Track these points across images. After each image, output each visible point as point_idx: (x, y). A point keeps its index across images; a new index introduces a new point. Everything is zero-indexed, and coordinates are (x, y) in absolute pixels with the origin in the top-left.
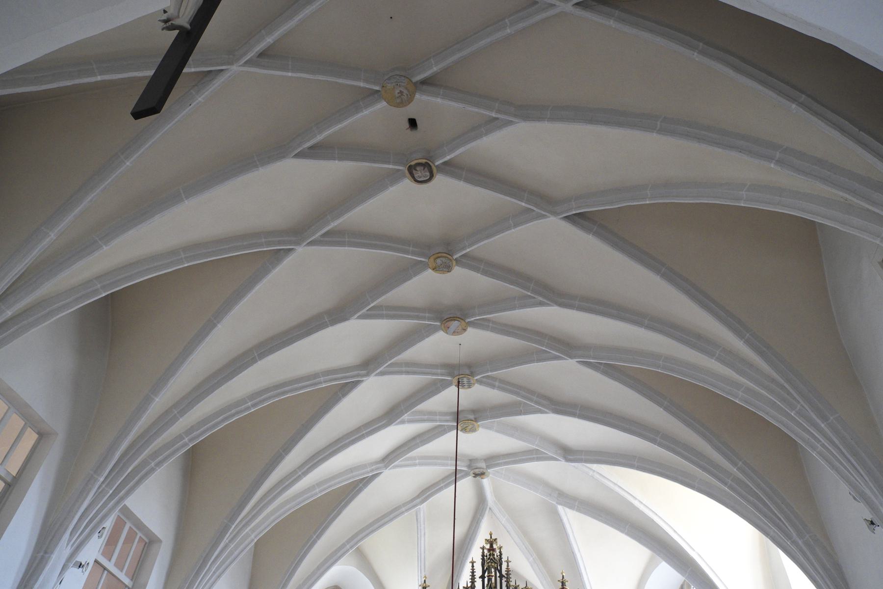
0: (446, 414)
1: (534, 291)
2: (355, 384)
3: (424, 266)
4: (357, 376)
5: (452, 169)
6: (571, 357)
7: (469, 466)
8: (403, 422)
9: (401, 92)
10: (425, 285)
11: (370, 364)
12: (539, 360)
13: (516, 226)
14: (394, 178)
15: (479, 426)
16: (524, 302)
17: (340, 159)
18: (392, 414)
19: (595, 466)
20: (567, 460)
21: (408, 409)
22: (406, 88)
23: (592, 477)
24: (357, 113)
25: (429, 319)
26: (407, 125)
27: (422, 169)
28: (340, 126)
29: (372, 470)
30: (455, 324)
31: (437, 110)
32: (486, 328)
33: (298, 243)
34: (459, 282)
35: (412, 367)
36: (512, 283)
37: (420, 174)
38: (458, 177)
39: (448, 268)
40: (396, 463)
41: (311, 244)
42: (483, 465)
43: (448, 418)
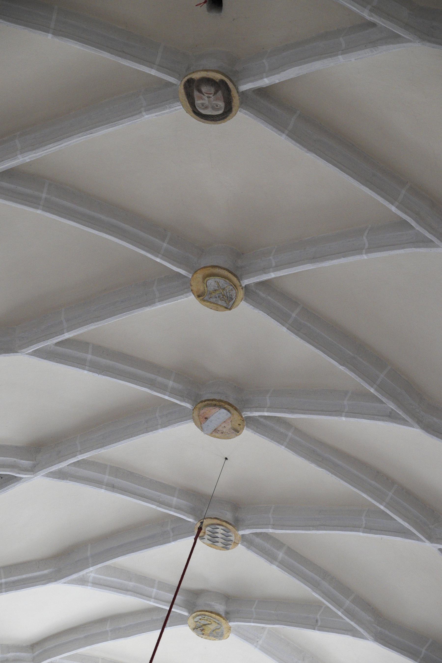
1: (381, 388)
6: (431, 538)
8: (83, 582)
10: (175, 323)
14: (154, 96)
25: (174, 392)
27: (212, 93)
30: (220, 415)
32: (279, 438)
35: (122, 478)
37: (206, 101)
38: (279, 125)
39: (228, 303)
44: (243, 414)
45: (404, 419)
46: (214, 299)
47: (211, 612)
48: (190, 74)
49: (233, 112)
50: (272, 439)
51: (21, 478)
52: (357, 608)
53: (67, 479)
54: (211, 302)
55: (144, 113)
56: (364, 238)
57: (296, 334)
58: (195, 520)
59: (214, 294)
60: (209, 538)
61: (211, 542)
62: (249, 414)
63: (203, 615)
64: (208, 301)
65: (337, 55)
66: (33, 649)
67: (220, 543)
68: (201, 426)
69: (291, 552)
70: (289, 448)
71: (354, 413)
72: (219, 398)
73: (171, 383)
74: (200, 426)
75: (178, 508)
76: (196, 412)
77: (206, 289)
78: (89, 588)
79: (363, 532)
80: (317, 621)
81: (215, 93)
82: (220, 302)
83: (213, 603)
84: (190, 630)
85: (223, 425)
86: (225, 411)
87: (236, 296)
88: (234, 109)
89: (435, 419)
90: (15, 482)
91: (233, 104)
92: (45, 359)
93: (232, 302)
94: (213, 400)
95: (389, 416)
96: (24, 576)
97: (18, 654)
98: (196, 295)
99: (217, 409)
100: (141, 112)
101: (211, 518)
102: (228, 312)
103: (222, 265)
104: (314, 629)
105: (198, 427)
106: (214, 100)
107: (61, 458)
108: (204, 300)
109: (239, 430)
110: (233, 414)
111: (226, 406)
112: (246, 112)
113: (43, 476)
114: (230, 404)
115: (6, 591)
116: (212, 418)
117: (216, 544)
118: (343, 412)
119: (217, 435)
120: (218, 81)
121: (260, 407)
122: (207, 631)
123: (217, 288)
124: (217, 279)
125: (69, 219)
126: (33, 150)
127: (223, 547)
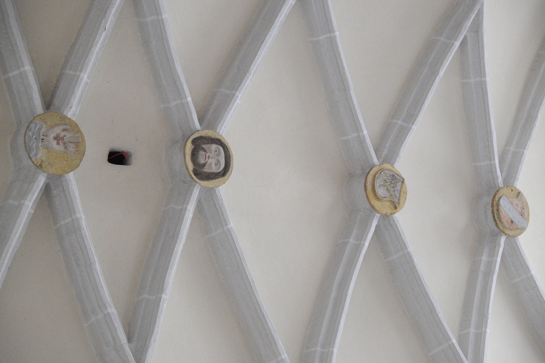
1: (453, 37)
5: (213, 106)
9: (57, 138)
13: (329, 28)
14: (211, 215)
16: (471, 63)
22: (52, 127)
24: (80, 229)
25: (492, 254)
26: (119, 146)
27: (204, 158)
28: (98, 266)
30: (506, 207)
32: (517, 158)
36: (434, 73)
37: (212, 161)
39: (396, 180)
44: (501, 187)
46: (396, 193)
48: (189, 172)
54: (400, 196)
55: (229, 226)
57: (417, 116)
59: (392, 192)
62: (500, 180)
64: (399, 199)
65: (162, 20)
68: (521, 229)
70: (525, 147)
71: (481, 71)
74: (523, 229)
77: (387, 199)
81: (205, 151)
82: (398, 187)
85: (516, 207)
86: (501, 202)
87: (390, 171)
93: (396, 176)
94: (493, 213)
95: (478, 32)
99: (501, 208)
100: (228, 230)
102: (406, 181)
103: (364, 180)
108: (399, 203)
109: (517, 192)
110: (503, 195)
111: (497, 199)
112: (219, 127)
116: (511, 217)
119: (526, 214)
120: (193, 147)
121: (492, 170)
123: (385, 188)
124: (377, 185)
125: (339, 323)
126: (275, 342)
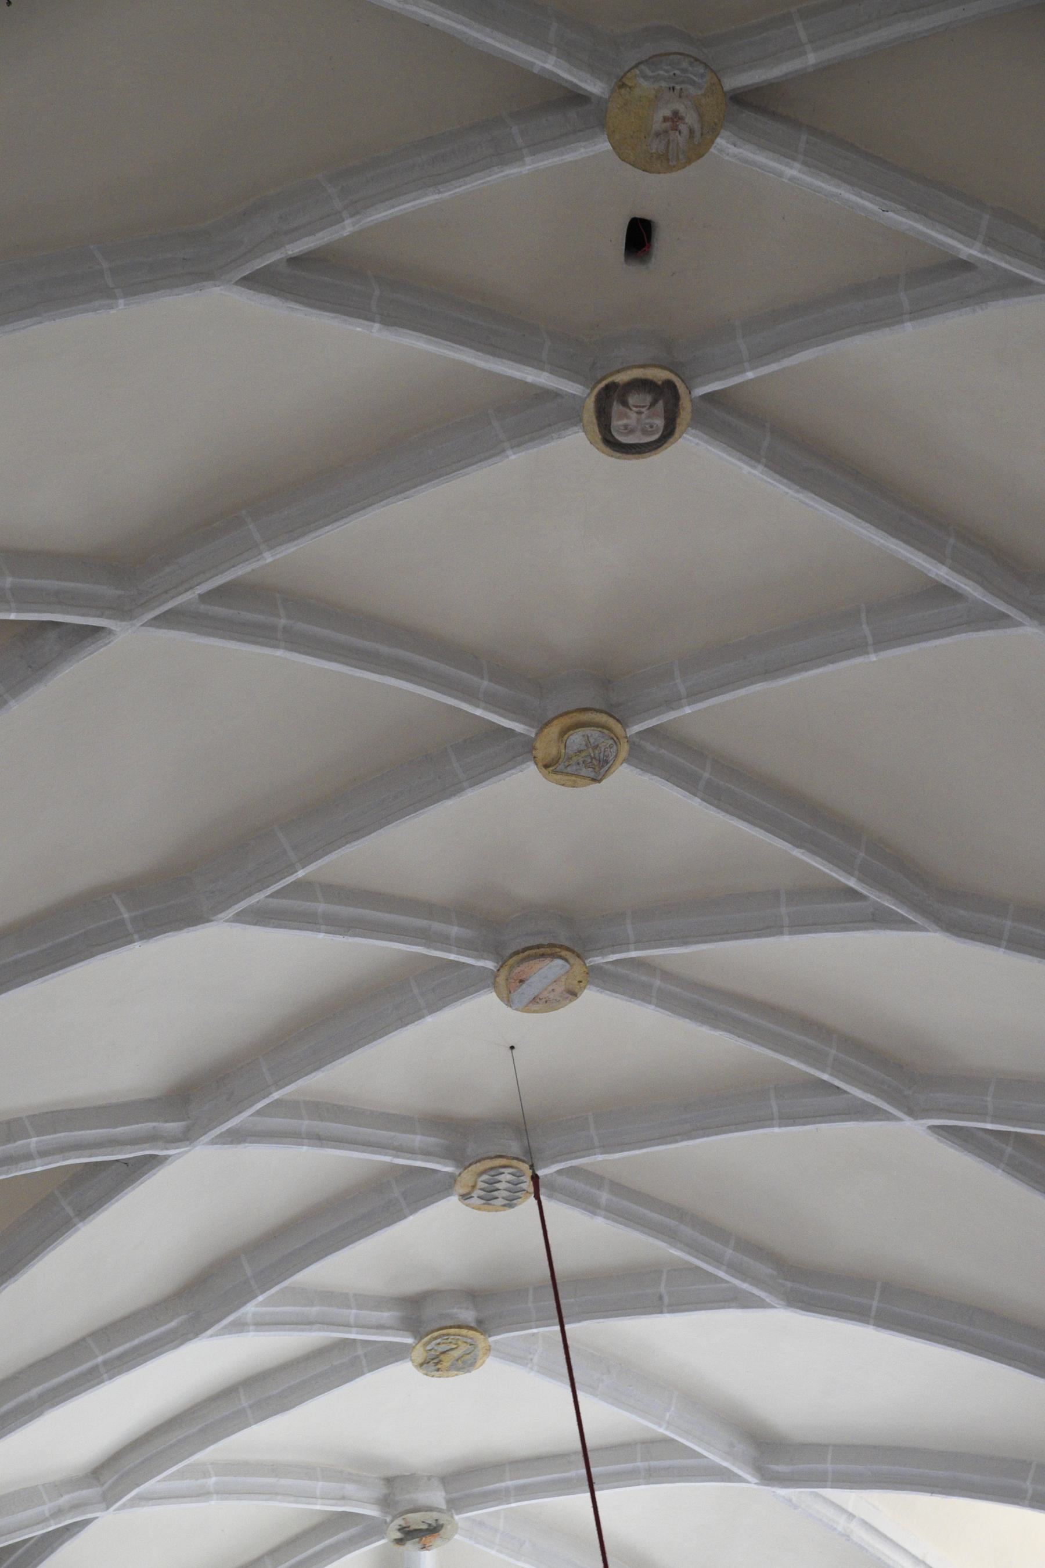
0: (379, 1302)
2: (135, 1170)
3: (515, 750)
4: (152, 1138)
5: (736, 422)
6: (913, 1112)
7: (386, 1503)
8: (239, 1327)
9: (676, 118)
10: (518, 822)
11: (200, 1098)
12: (789, 1119)
13: (882, 643)
14: (529, 417)
15: (488, 1350)
17: (389, 320)
18: (202, 1296)
19: (852, 1499)
20: (768, 1478)
21: (266, 1279)
23: (847, 1537)
27: (638, 405)
28: (431, 198)
29: (58, 1513)
30: (549, 972)
31: (764, 198)
32: (639, 992)
33: (124, 611)
34: (643, 817)
35: (332, 1121)
36: (798, 839)
38: (749, 450)
39: (598, 767)
40: (151, 1485)
41: (170, 619)
42: (437, 1497)
43: (386, 1316)
44: (587, 961)
45: (911, 922)
47: (459, 1327)
48: (612, 374)
49: (676, 435)
50: (633, 997)
51: (166, 1158)
52: (746, 1259)
53: (245, 1141)
54: (567, 774)
56: (864, 626)
58: (457, 1167)
60: (482, 1193)
61: (483, 1201)
62: (598, 960)
63: (444, 1335)
64: (562, 773)
66: (98, 1479)
67: (500, 1199)
69: (618, 1188)
71: (802, 925)
72: (534, 941)
73: (454, 930)
75: (427, 1153)
76: (504, 973)
78: (252, 1334)
79: (780, 1126)
80: (661, 1298)
81: (653, 404)
82: (584, 772)
83: (455, 1310)
84: (414, 1369)
85: (550, 988)
86: (559, 962)
87: (616, 756)
88: (678, 430)
89: (962, 912)
90: (157, 1166)
91: (678, 421)
92: (255, 924)
94: (538, 947)
95: (874, 920)
96: (136, 1342)
97: (76, 1494)
98: (540, 764)
99: (547, 961)
101: (491, 1158)
104: (661, 1312)
105: (502, 999)
106: (648, 417)
107: (237, 1105)
108: (555, 772)
110: (571, 966)
111: (564, 953)
113: (207, 1144)
114: (568, 949)
115: (110, 1378)
117: (492, 1202)
118: (782, 927)
120: (660, 383)
122: (446, 1364)
123: (582, 748)
124: (588, 731)
125: (330, 660)
127: (504, 1205)
